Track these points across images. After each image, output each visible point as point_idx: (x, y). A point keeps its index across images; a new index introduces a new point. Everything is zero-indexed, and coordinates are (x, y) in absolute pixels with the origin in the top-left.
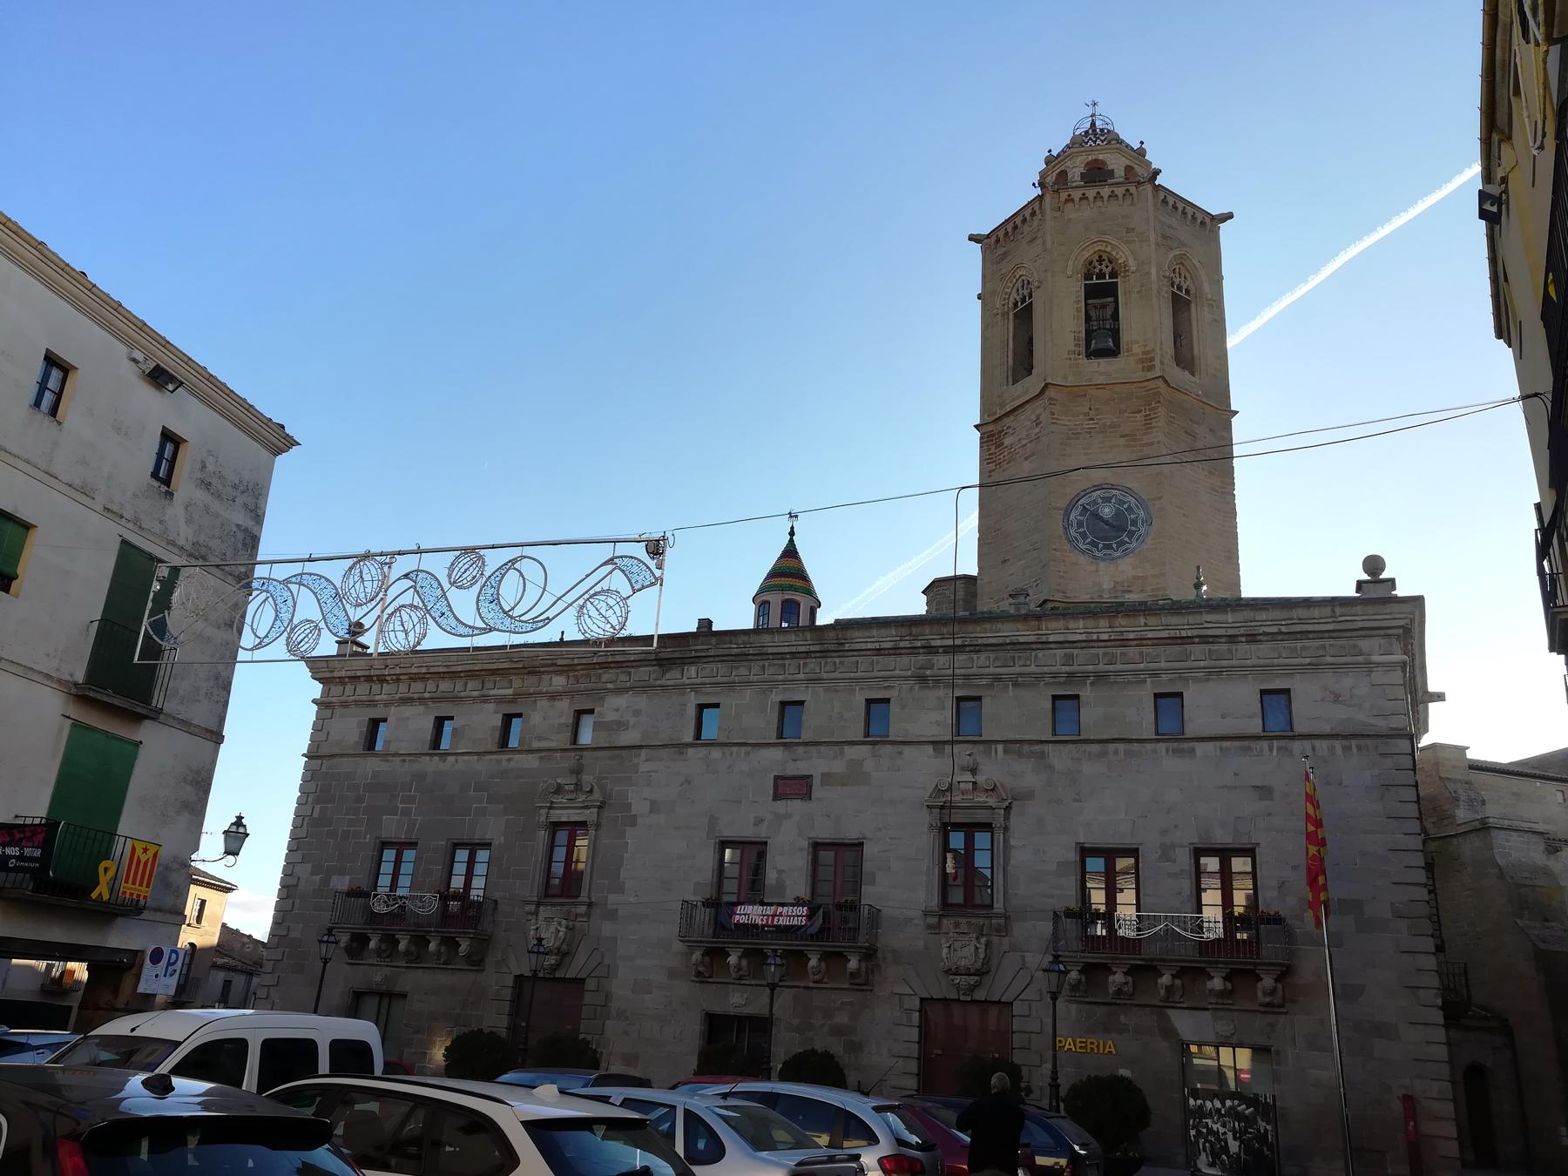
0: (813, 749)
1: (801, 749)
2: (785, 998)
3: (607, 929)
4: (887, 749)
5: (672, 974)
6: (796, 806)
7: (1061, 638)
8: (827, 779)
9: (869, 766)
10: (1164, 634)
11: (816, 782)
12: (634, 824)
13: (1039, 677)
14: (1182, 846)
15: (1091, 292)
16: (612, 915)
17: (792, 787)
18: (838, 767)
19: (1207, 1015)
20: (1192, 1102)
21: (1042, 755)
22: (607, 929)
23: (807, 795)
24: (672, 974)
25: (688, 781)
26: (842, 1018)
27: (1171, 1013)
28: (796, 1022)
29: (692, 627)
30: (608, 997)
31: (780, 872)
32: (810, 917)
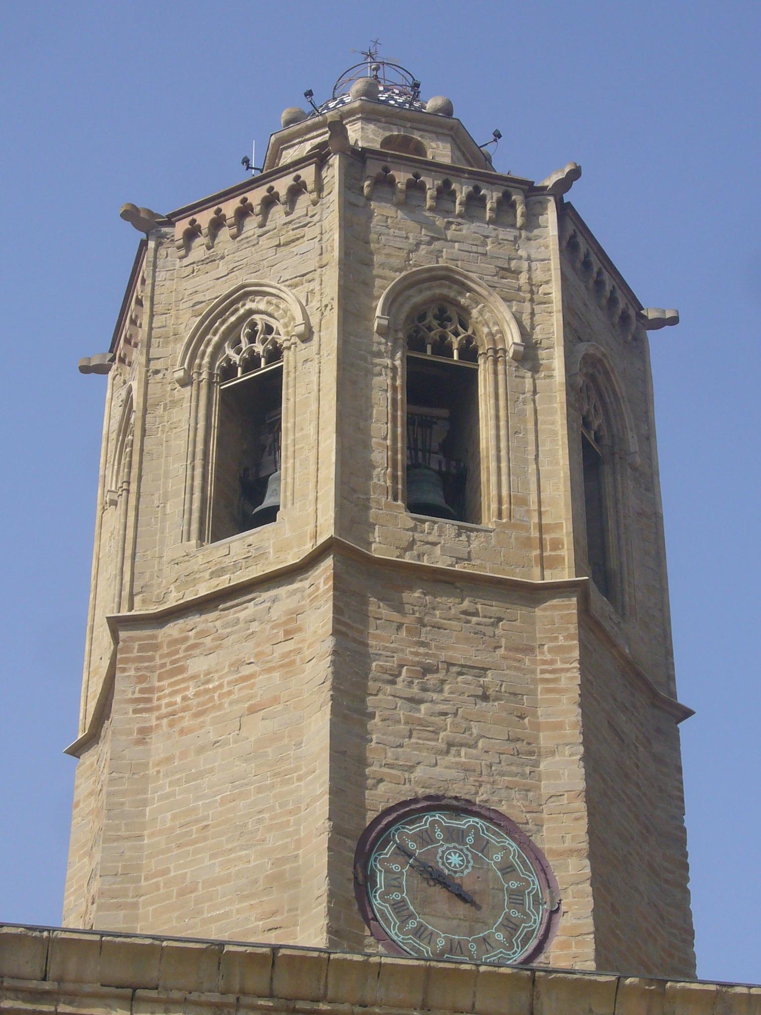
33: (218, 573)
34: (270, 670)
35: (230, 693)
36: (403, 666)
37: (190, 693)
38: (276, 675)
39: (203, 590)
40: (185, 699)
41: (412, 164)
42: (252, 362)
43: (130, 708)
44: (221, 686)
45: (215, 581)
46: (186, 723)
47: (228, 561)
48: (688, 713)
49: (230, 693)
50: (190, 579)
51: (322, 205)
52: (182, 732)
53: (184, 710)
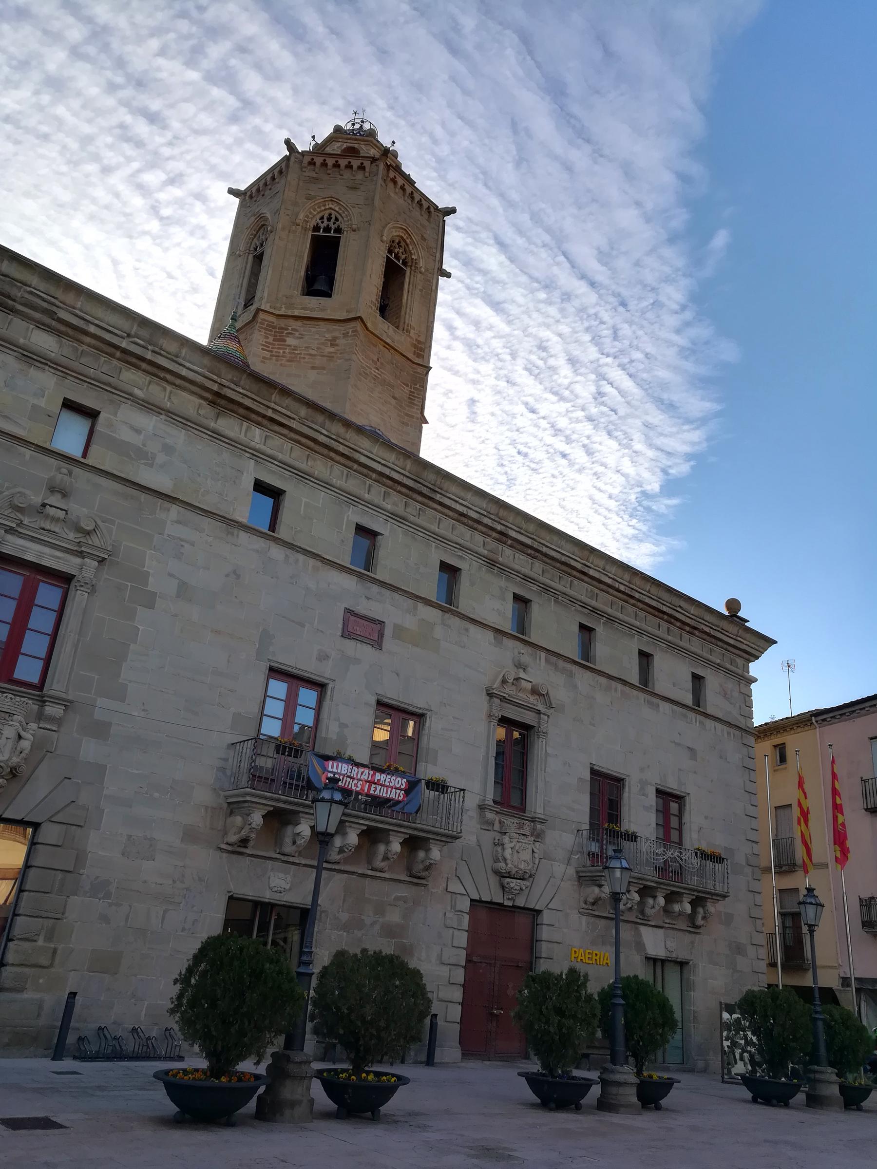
0: (387, 593)
1: (375, 589)
2: (334, 886)
3: (90, 750)
4: (456, 621)
5: (190, 835)
6: (365, 651)
7: (596, 575)
8: (400, 632)
9: (439, 632)
10: (654, 603)
11: (388, 632)
12: (151, 606)
13: (573, 600)
14: (651, 785)
15: (317, 242)
16: (100, 730)
17: (362, 628)
18: (409, 622)
19: (661, 932)
20: (726, 1016)
21: (571, 675)
22: (90, 750)
23: (378, 644)
24: (190, 835)
25: (236, 574)
26: (394, 917)
27: (643, 929)
28: (344, 917)
29: (426, 414)
30: (80, 858)
31: (343, 726)
32: (408, 791)
33: (305, 309)
34: (323, 356)
35: (304, 358)
36: (492, 1014)
37: (287, 351)
38: (325, 358)
39: (296, 313)
40: (284, 352)
41: (545, 559)
42: (327, 229)
43: (261, 347)
44: (300, 354)
45: (303, 311)
46: (283, 362)
47: (309, 306)
48: (755, 680)
49: (304, 358)
50: (291, 306)
51: (333, 343)
52: (281, 365)
53: (283, 356)
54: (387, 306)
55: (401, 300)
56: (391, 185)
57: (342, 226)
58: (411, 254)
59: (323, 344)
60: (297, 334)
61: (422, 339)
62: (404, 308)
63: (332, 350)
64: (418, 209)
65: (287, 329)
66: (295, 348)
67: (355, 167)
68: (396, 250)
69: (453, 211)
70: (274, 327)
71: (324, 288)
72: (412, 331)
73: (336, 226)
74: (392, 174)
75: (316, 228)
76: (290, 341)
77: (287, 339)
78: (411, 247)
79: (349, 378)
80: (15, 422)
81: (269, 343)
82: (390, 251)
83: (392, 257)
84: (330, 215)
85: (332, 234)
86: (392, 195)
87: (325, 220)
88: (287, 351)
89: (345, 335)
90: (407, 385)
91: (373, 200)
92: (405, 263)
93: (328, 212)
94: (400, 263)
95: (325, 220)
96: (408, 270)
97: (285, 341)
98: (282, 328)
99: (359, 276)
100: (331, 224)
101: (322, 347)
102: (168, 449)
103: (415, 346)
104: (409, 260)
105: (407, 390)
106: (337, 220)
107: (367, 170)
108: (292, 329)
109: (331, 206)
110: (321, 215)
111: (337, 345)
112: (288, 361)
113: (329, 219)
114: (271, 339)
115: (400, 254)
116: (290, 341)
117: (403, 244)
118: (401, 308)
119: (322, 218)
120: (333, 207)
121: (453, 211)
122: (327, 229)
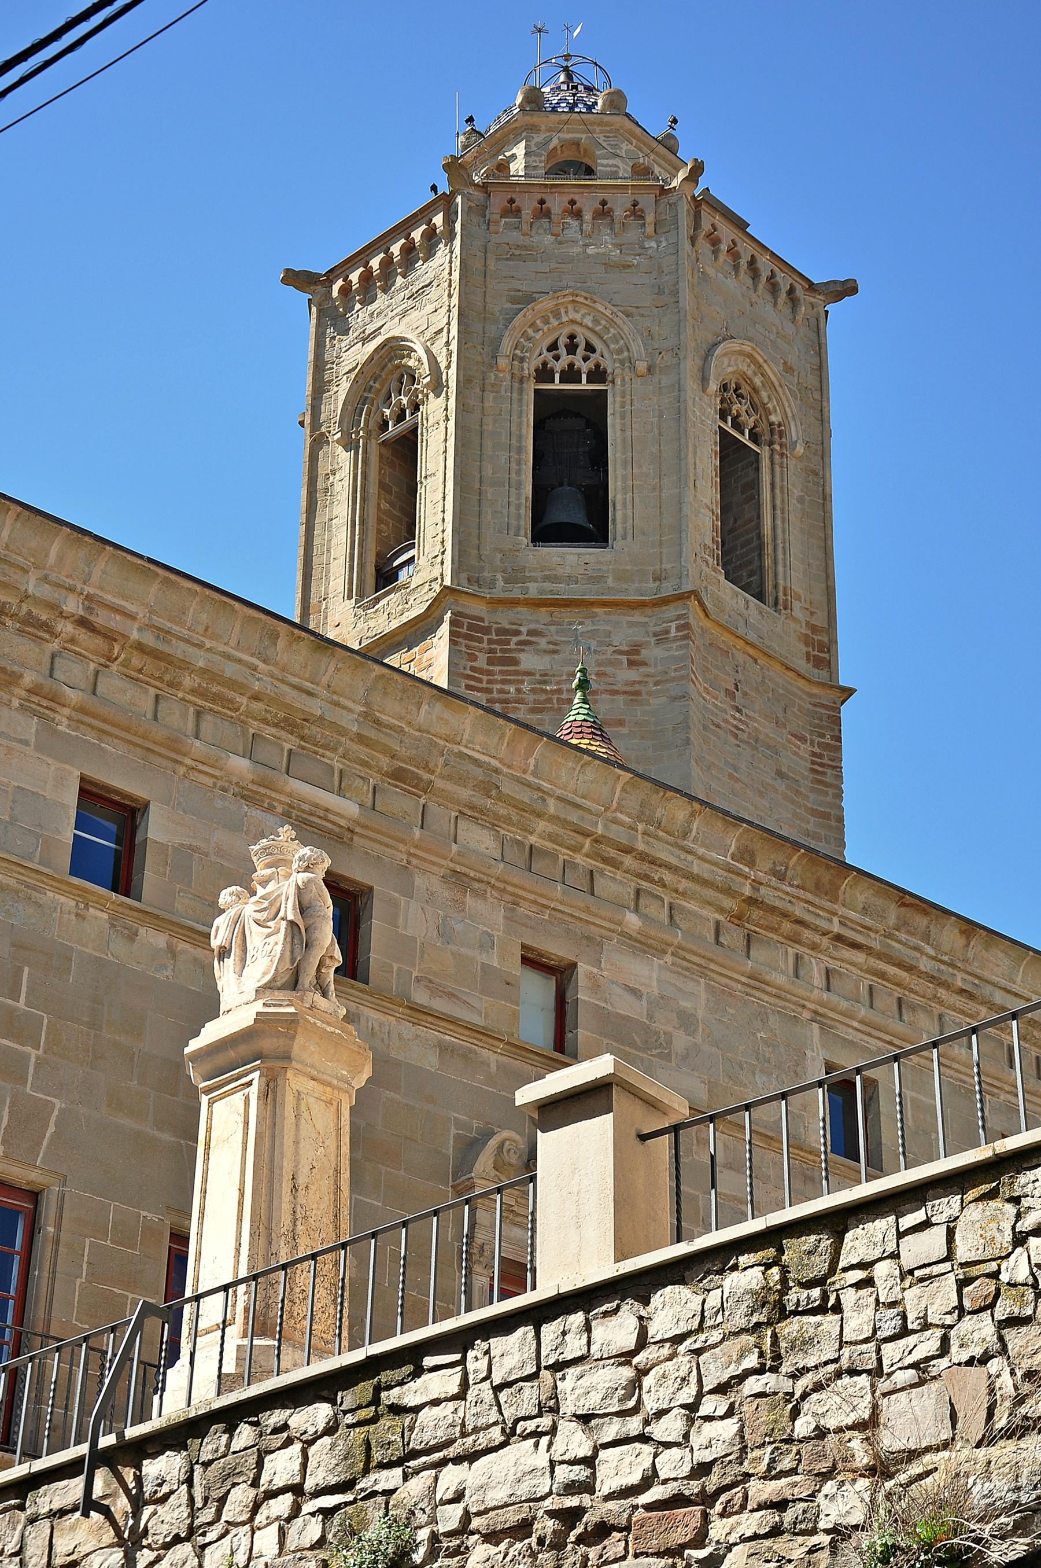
37: (526, 687)
38: (621, 698)
40: (519, 691)
42: (571, 375)
44: (559, 691)
45: (548, 586)
51: (633, 657)
54: (742, 554)
55: (758, 527)
56: (704, 246)
57: (607, 364)
58: (768, 412)
59: (611, 663)
60: (543, 643)
61: (820, 620)
62: (769, 550)
63: (633, 675)
64: (768, 297)
65: (517, 633)
66: (545, 677)
67: (619, 213)
68: (735, 408)
69: (847, 289)
70: (487, 631)
71: (577, 516)
72: (797, 605)
73: (590, 365)
74: (708, 219)
75: (544, 374)
76: (528, 660)
77: (522, 656)
78: (764, 394)
79: (688, 742)
80: (465, 1002)
81: (480, 671)
82: (723, 415)
83: (728, 428)
84: (572, 337)
85: (584, 385)
86: (711, 271)
87: (562, 351)
88: (526, 687)
89: (661, 637)
90: (803, 739)
91: (675, 293)
92: (754, 437)
93: (566, 331)
94: (745, 439)
95: (562, 351)
96: (764, 452)
97: (515, 662)
98: (501, 631)
99: (662, 480)
100: (578, 360)
101: (609, 670)
102: (687, 1021)
103: (807, 641)
104: (763, 427)
105: (805, 750)
106: (590, 348)
107: (650, 218)
108: (530, 633)
109: (572, 315)
110: (549, 340)
111: (644, 664)
112: (533, 711)
113: (572, 349)
114: (481, 662)
115: (744, 417)
116: (528, 660)
117: (745, 390)
118: (761, 547)
119: (553, 347)
120: (578, 317)
121: (847, 289)
122: (571, 375)
